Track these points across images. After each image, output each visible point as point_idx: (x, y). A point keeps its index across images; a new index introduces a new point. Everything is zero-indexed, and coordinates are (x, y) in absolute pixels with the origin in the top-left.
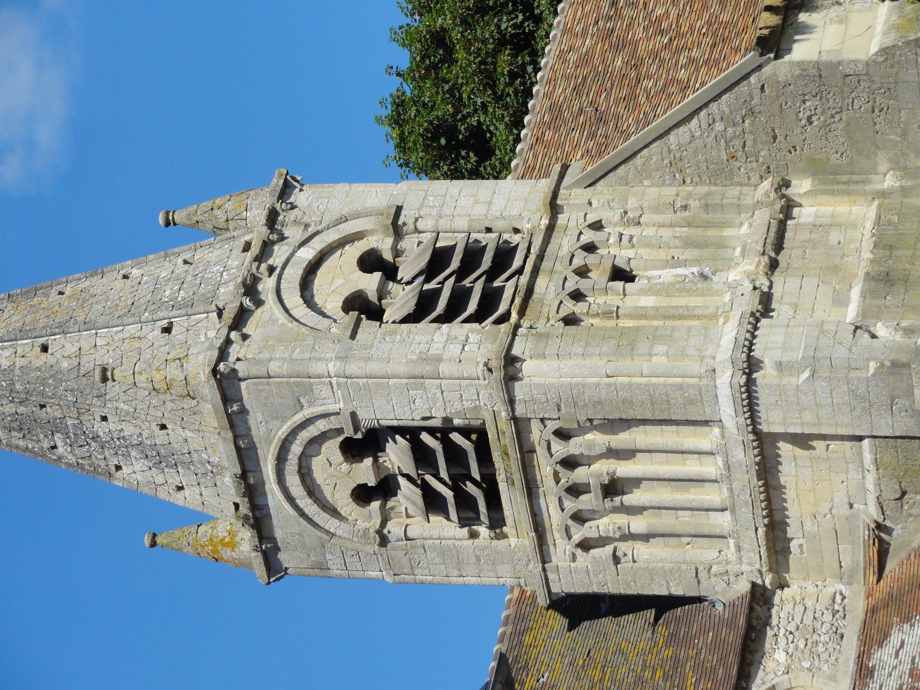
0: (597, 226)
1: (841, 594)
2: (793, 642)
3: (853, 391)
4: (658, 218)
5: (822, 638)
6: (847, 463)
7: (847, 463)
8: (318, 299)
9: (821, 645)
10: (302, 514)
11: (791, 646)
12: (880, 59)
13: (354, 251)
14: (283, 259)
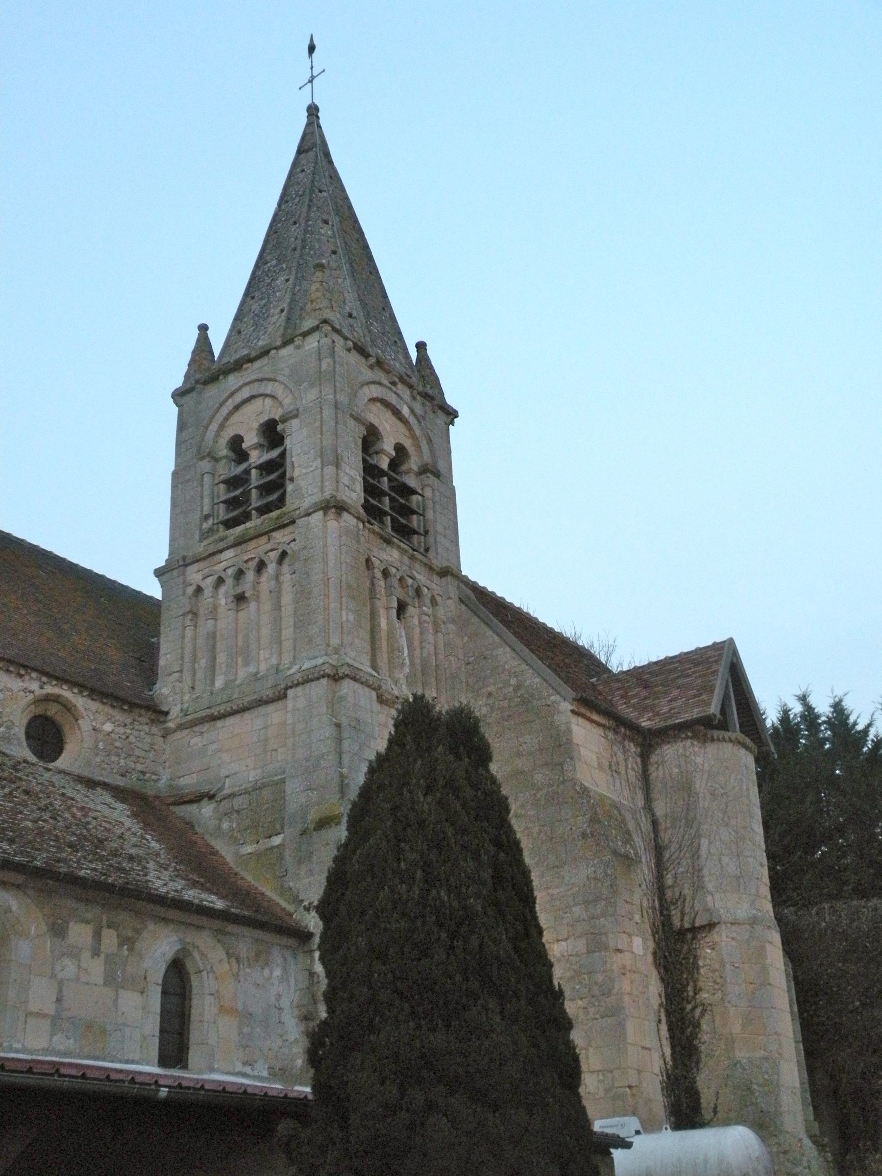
0: (434, 602)
1: (159, 779)
2: (119, 737)
3: (323, 756)
4: (441, 644)
5: (122, 761)
6: (262, 767)
7: (262, 767)
8: (379, 405)
9: (117, 759)
10: (222, 404)
11: (117, 737)
12: (578, 788)
13: (408, 443)
14: (400, 393)
